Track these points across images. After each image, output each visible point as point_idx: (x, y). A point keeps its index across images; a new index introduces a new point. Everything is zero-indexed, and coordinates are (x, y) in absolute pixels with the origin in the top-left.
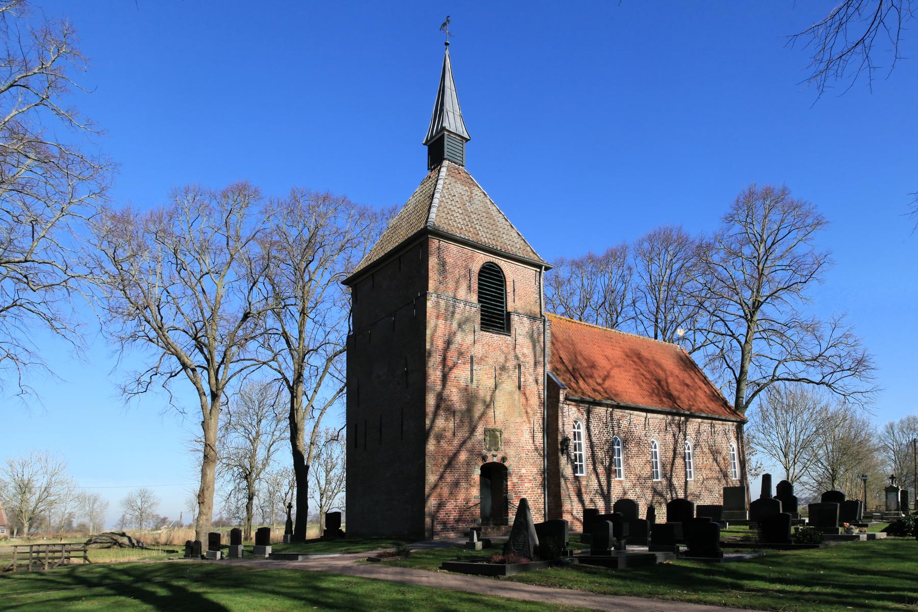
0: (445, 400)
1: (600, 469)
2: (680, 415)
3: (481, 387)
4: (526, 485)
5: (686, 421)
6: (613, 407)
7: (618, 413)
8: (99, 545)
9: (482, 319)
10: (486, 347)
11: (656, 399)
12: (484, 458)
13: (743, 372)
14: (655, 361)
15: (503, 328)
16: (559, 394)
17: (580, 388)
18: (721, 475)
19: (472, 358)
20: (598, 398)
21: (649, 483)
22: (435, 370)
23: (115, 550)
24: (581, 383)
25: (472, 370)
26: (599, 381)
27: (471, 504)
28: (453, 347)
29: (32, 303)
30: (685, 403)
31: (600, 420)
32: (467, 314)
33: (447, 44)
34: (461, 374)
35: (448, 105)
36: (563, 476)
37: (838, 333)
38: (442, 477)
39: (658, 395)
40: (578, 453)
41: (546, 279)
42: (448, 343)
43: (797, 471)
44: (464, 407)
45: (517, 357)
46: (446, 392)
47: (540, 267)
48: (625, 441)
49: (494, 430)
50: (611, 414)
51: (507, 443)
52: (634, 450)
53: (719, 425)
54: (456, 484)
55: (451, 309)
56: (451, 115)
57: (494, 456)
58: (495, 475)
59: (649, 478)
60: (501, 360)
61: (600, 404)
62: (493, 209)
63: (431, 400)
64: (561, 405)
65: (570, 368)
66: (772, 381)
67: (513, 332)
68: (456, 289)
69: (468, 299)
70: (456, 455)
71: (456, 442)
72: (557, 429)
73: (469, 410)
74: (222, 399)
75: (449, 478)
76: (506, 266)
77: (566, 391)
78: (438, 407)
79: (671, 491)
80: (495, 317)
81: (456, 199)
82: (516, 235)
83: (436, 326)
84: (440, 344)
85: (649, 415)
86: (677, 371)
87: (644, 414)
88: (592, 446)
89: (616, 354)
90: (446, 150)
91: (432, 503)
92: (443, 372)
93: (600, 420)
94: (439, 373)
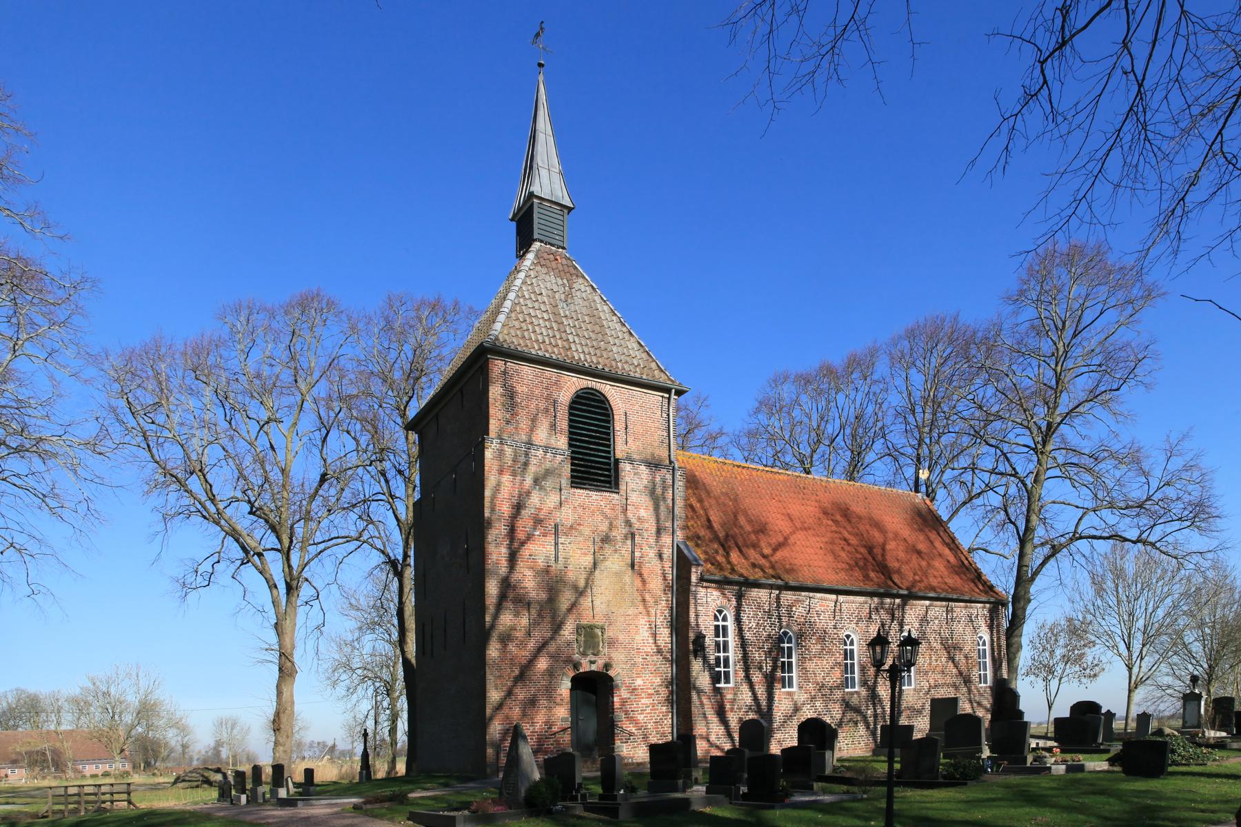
0: (515, 587)
1: (757, 677)
2: (894, 596)
3: (570, 567)
4: (643, 701)
5: (904, 604)
6: (780, 588)
7: (788, 597)
8: (186, 784)
9: (572, 470)
10: (580, 510)
11: (857, 573)
12: (576, 666)
13: (1028, 529)
14: (871, 519)
15: (610, 482)
16: (690, 572)
17: (729, 563)
18: (959, 681)
19: (556, 526)
20: (757, 575)
21: (838, 694)
22: (498, 545)
23: (205, 789)
24: (734, 556)
25: (556, 544)
26: (767, 551)
27: (555, 729)
28: (525, 513)
29: (18, 476)
30: (907, 575)
31: (759, 607)
32: (548, 465)
33: (540, 65)
34: (539, 550)
35: (540, 159)
36: (695, 688)
37: (1177, 463)
38: (510, 693)
39: (864, 569)
40: (722, 655)
41: (678, 410)
42: (518, 508)
43: (1144, 669)
44: (544, 596)
45: (628, 523)
46: (516, 576)
47: (668, 391)
48: (800, 636)
49: (591, 627)
50: (778, 598)
51: (612, 643)
52: (815, 648)
53: (960, 610)
54: (532, 702)
55: (522, 459)
56: (544, 173)
57: (592, 662)
58: (595, 690)
59: (838, 687)
60: (604, 527)
61: (757, 585)
62: (604, 310)
63: (492, 588)
64: (693, 589)
65: (721, 535)
66: (1071, 540)
67: (622, 487)
68: (532, 429)
69: (552, 442)
70: (532, 661)
71: (532, 644)
72: (688, 623)
73: (552, 600)
74: (305, 592)
75: (521, 694)
76: (615, 394)
77: (700, 569)
78: (502, 597)
79: (874, 705)
80: (593, 464)
81: (535, 302)
82: (636, 346)
83: (499, 485)
84: (505, 509)
85: (841, 598)
86: (906, 532)
87: (834, 597)
88: (743, 644)
89: (806, 510)
90: (536, 226)
91: (495, 728)
92: (510, 547)
93: (759, 607)
94: (504, 550)
